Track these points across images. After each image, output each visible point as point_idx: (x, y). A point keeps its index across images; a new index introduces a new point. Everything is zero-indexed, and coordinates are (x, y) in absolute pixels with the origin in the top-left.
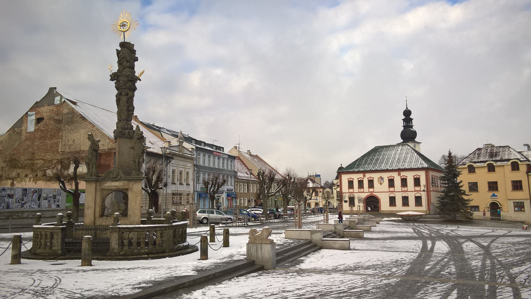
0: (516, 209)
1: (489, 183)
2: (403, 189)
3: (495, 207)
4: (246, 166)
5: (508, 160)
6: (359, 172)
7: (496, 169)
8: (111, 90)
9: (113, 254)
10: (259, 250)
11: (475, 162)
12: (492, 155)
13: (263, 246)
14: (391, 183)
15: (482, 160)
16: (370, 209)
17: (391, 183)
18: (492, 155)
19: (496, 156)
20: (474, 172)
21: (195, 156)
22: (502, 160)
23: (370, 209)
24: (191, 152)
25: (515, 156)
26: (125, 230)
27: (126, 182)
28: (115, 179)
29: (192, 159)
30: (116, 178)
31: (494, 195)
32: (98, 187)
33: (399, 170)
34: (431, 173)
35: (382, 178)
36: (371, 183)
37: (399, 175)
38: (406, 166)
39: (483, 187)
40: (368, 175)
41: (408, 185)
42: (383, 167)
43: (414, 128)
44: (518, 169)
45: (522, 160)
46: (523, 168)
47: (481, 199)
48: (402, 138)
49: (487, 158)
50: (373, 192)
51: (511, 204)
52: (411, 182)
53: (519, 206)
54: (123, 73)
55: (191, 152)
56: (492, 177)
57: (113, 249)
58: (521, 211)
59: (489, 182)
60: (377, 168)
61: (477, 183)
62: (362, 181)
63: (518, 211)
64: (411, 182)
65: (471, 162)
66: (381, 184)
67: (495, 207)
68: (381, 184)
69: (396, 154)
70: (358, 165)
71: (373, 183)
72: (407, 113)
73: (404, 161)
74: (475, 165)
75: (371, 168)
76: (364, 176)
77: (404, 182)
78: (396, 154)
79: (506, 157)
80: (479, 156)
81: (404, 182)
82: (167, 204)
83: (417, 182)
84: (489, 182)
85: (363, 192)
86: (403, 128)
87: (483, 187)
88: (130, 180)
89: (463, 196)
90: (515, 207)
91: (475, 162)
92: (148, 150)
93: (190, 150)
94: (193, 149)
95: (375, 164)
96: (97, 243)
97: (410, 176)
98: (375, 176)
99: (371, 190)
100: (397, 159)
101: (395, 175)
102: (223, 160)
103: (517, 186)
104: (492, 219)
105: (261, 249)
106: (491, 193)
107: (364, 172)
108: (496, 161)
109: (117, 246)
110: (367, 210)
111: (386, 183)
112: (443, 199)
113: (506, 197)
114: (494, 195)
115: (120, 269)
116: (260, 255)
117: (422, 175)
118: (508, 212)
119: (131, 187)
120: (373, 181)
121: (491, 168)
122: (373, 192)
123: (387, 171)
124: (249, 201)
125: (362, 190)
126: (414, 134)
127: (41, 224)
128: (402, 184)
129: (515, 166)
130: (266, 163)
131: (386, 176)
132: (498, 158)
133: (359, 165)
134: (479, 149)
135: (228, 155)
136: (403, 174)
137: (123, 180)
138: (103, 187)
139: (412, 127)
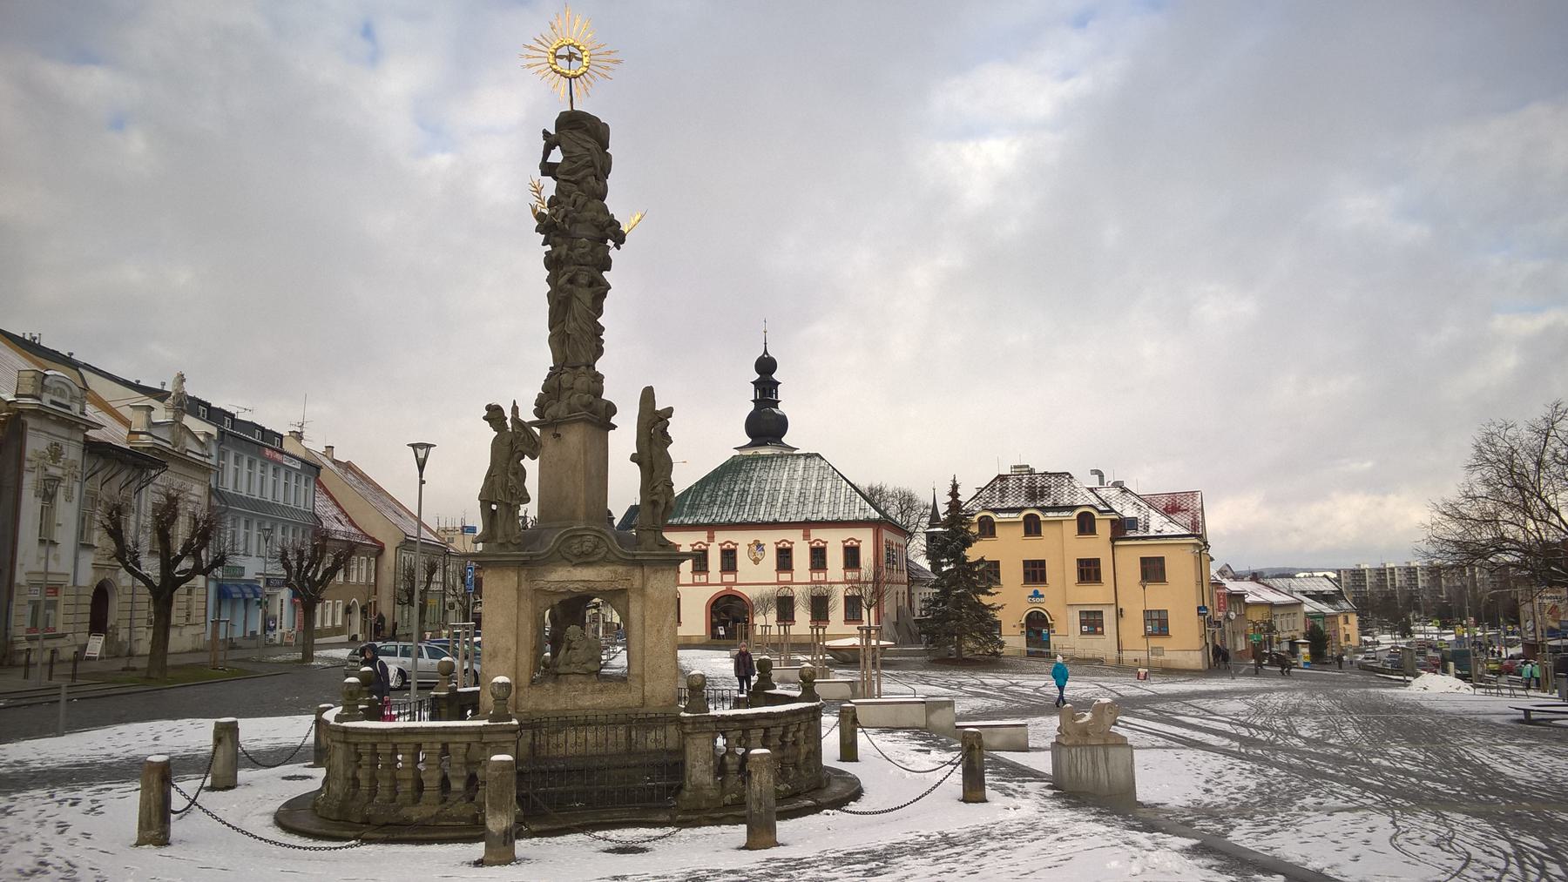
0: (1085, 628)
1: (1042, 563)
2: (815, 576)
3: (1037, 625)
4: (332, 498)
5: (1072, 508)
6: (697, 527)
7: (1044, 529)
8: (529, 261)
9: (704, 805)
10: (1102, 765)
11: (996, 511)
12: (1035, 493)
13: (1112, 752)
14: (784, 558)
15: (1010, 505)
16: (722, 632)
17: (784, 558)
18: (1035, 493)
19: (1042, 496)
20: (1038, 532)
21: (213, 461)
22: (1056, 508)
23: (722, 632)
24: (201, 444)
25: (1084, 499)
26: (730, 724)
27: (621, 569)
28: (584, 560)
29: (205, 469)
30: (588, 555)
31: (1036, 594)
32: (524, 585)
33: (807, 525)
34: (886, 535)
35: (759, 546)
36: (729, 560)
37: (806, 536)
38: (825, 514)
39: (1012, 574)
40: (722, 537)
41: (795, 567)
42: (762, 515)
43: (783, 408)
44: (1092, 531)
45: (1101, 508)
46: (1103, 528)
47: (1010, 601)
48: (749, 433)
49: (1021, 502)
50: (735, 583)
51: (1076, 618)
52: (835, 558)
53: (1092, 622)
54: (587, 215)
55: (201, 444)
56: (1033, 549)
57: (698, 788)
58: (1096, 633)
59: (1025, 563)
60: (744, 516)
61: (997, 563)
62: (705, 552)
63: (1088, 633)
64: (835, 558)
65: (985, 509)
66: (756, 561)
67: (1037, 625)
68: (756, 561)
69: (791, 479)
70: (691, 506)
71: (735, 558)
72: (766, 366)
73: (818, 500)
74: (996, 518)
75: (729, 515)
76: (711, 538)
77: (818, 557)
78: (791, 479)
79: (1066, 501)
80: (1003, 496)
81: (818, 557)
82: (136, 623)
83: (852, 556)
84: (1025, 563)
85: (707, 584)
86: (752, 407)
87: (1012, 574)
88: (640, 564)
89: (981, 597)
90: (1082, 623)
91: (996, 511)
92: (90, 433)
93: (201, 438)
94: (208, 435)
95: (740, 506)
96: (543, 772)
97: (835, 542)
98: (742, 541)
99: (729, 578)
100: (797, 494)
101: (795, 537)
102: (287, 475)
103: (1089, 572)
104: (1030, 654)
105: (1107, 759)
106: (1030, 590)
107: (712, 528)
108: (1044, 509)
109: (708, 779)
110: (715, 635)
111: (770, 558)
112: (936, 603)
113: (1063, 598)
114: (1036, 594)
115: (948, 841)
116: (1103, 776)
117: (866, 540)
118: (1067, 637)
119: (637, 583)
120: (734, 552)
121: (1032, 527)
122: (735, 583)
123: (775, 525)
124: (348, 610)
125: (703, 578)
126: (781, 424)
127: (392, 718)
128: (812, 563)
129: (1086, 525)
130: (379, 489)
131: (770, 539)
132: (1048, 503)
133: (694, 508)
134: (1002, 478)
135: (303, 461)
136: (816, 534)
137: (613, 563)
138: (541, 584)
139: (775, 403)
